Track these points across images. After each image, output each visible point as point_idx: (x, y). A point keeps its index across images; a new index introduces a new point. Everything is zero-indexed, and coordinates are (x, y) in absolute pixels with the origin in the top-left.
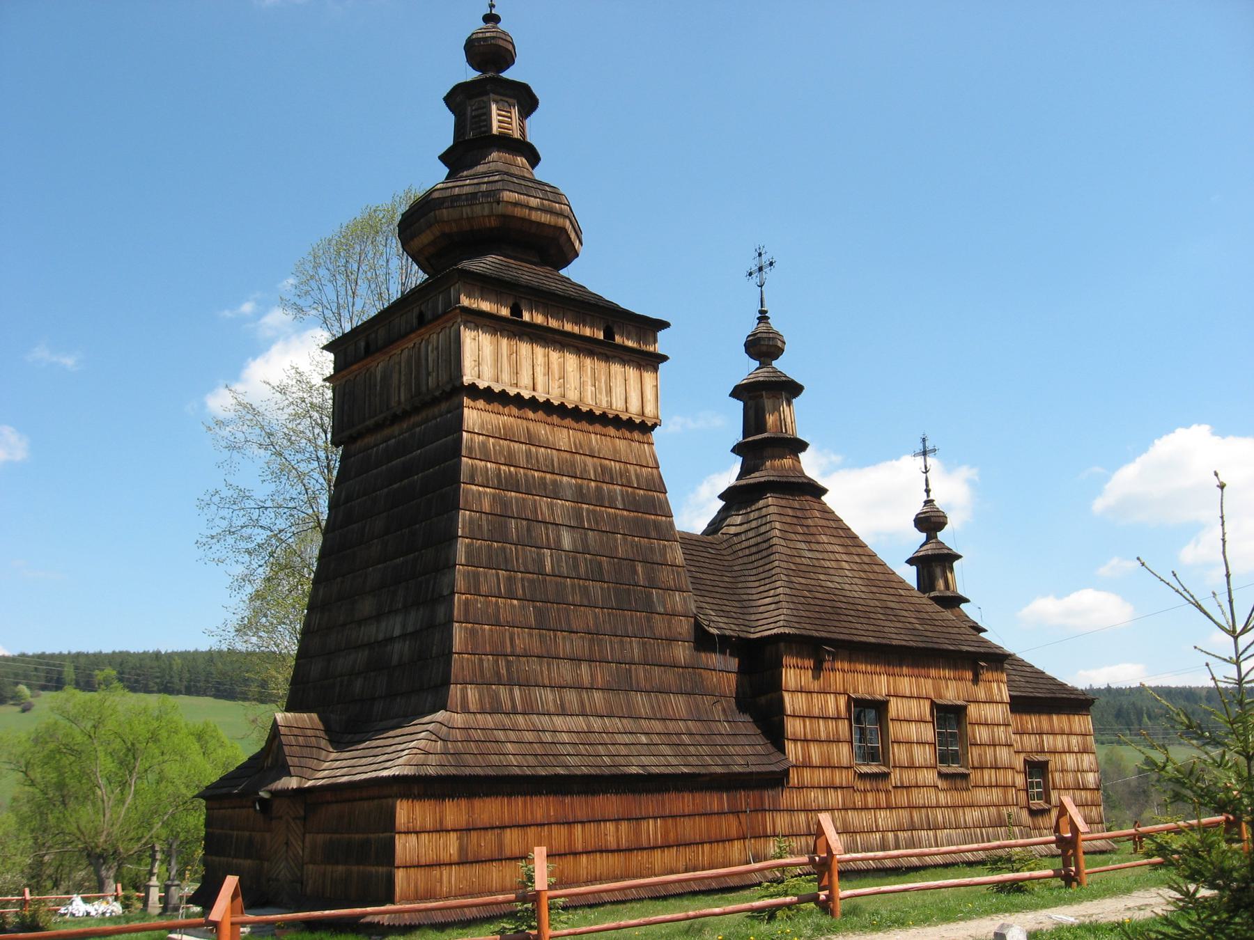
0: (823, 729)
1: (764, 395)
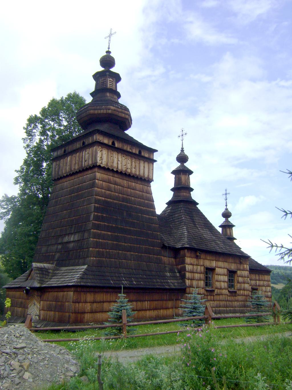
0: (197, 276)
1: (182, 173)
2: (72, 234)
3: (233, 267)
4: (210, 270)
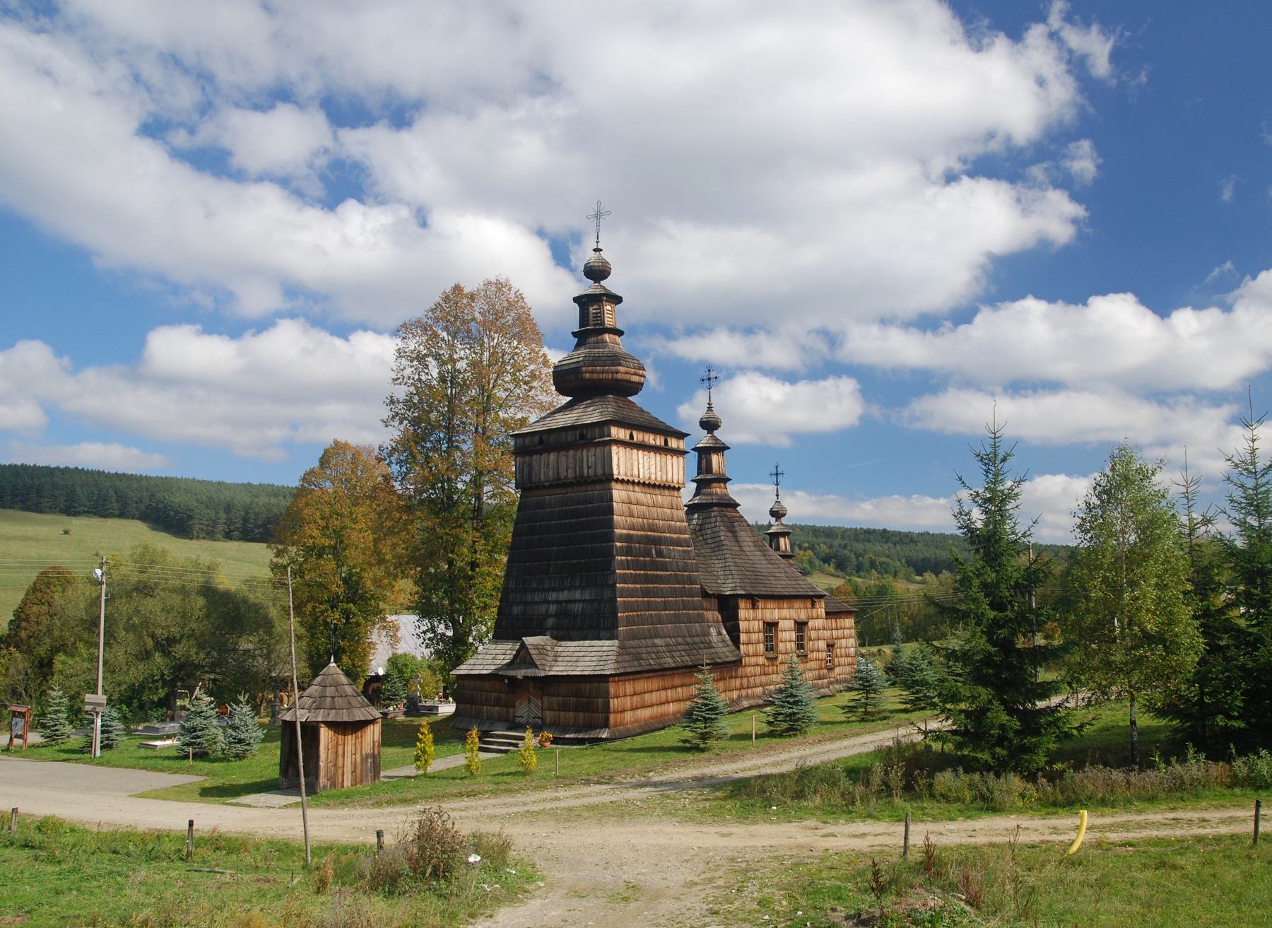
2: (576, 588)
3: (803, 615)
4: (771, 626)
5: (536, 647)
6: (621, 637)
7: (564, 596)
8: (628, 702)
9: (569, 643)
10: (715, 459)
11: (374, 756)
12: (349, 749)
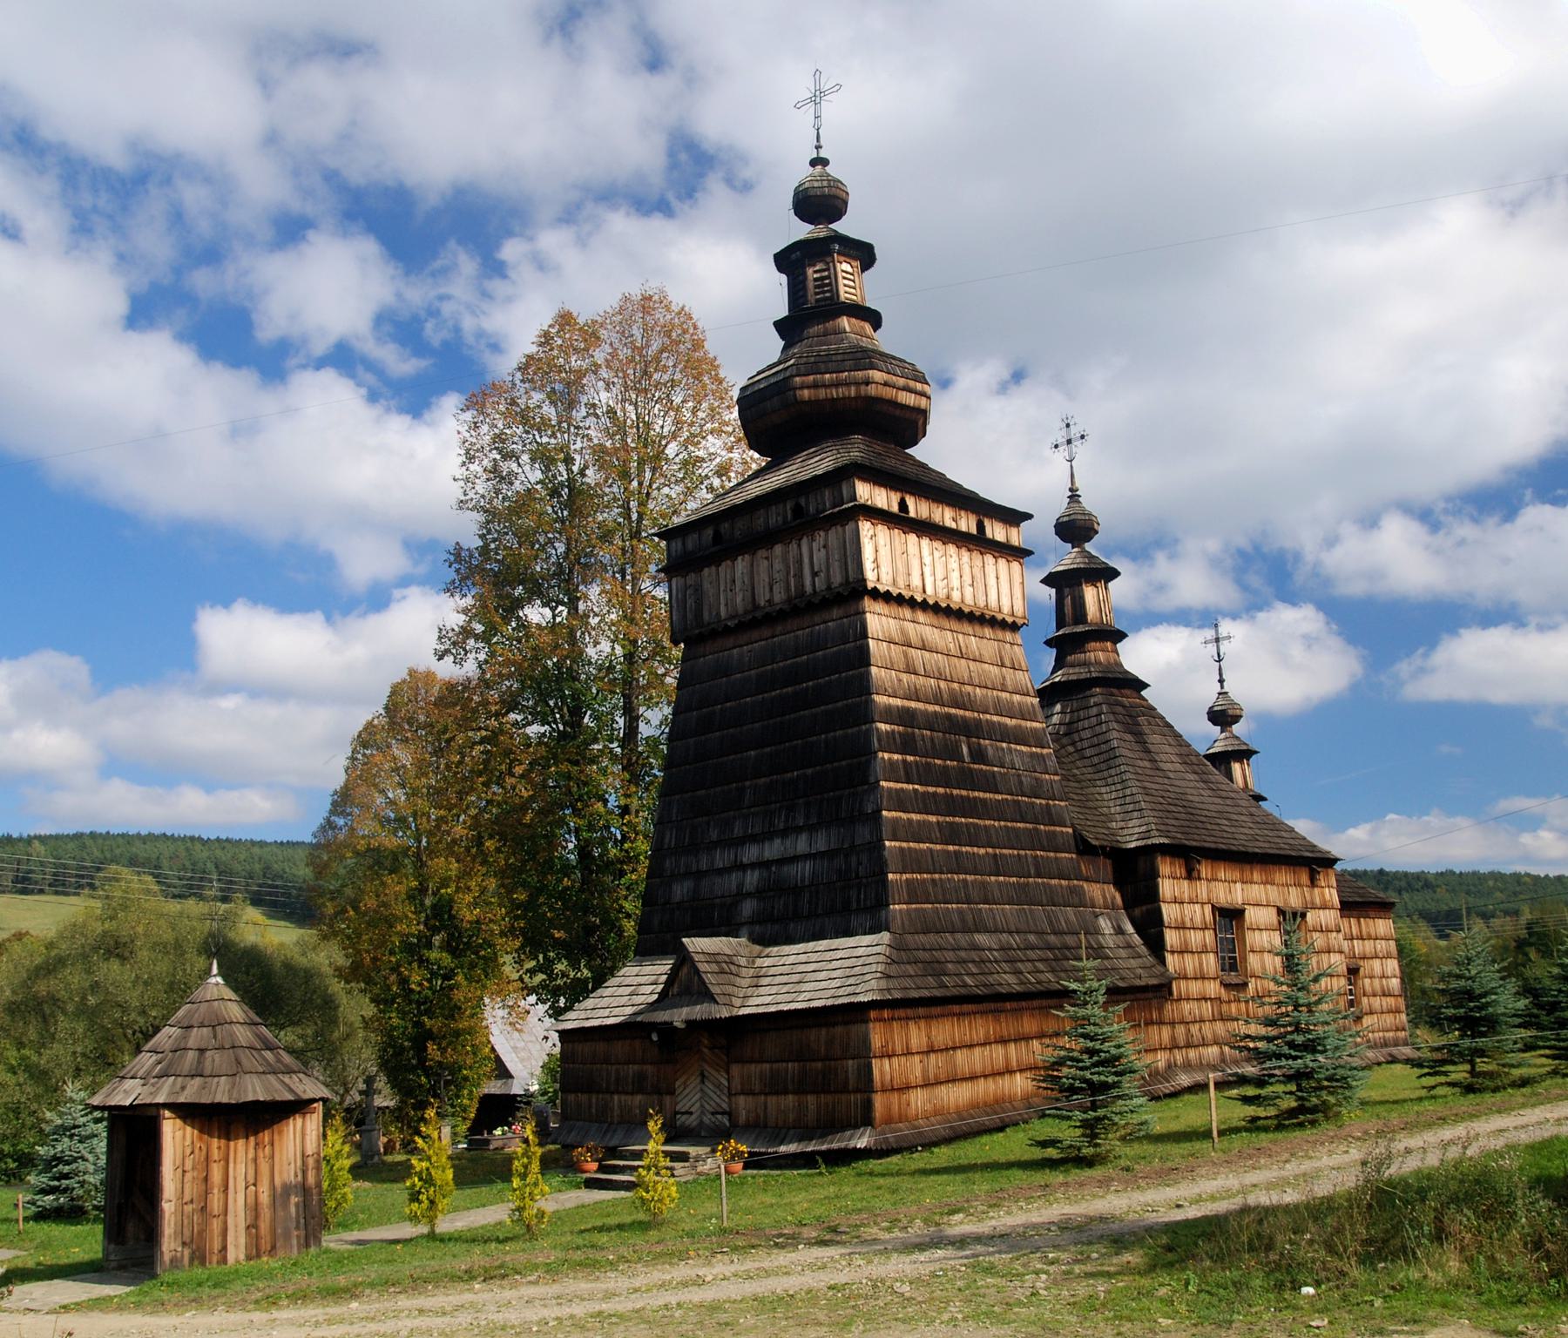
2: (798, 830)
3: (1294, 899)
4: (1230, 917)
5: (713, 957)
6: (896, 924)
7: (773, 849)
8: (915, 1068)
9: (786, 949)
10: (1090, 594)
11: (304, 1189)
12: (240, 1170)
